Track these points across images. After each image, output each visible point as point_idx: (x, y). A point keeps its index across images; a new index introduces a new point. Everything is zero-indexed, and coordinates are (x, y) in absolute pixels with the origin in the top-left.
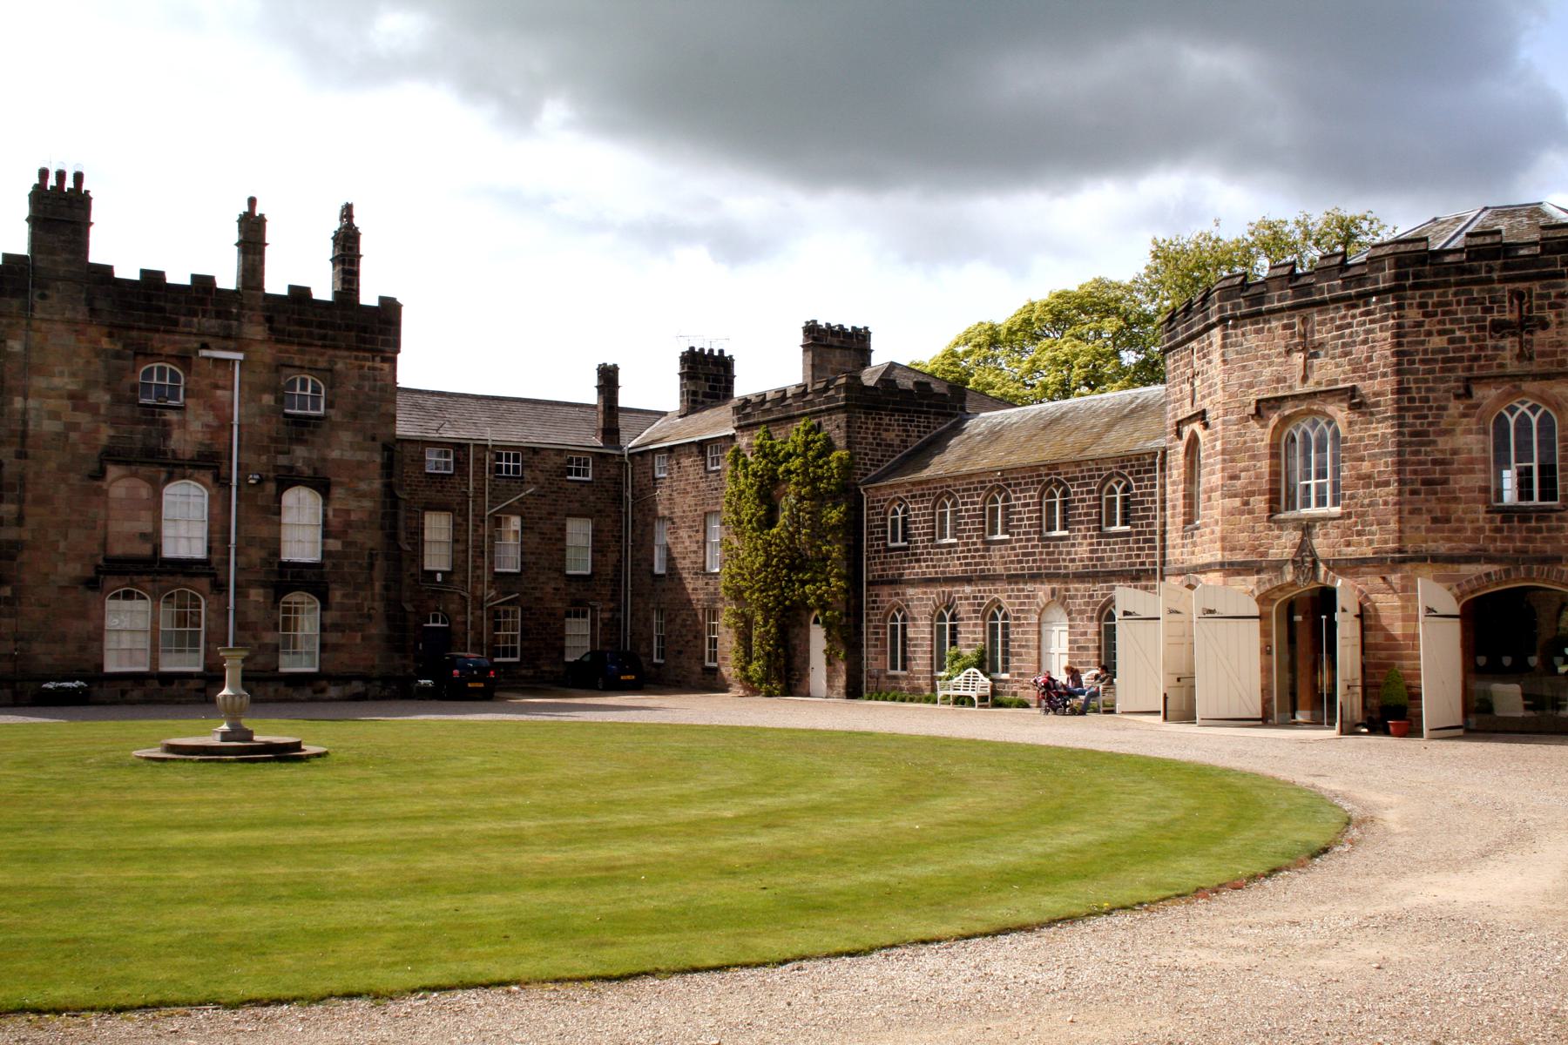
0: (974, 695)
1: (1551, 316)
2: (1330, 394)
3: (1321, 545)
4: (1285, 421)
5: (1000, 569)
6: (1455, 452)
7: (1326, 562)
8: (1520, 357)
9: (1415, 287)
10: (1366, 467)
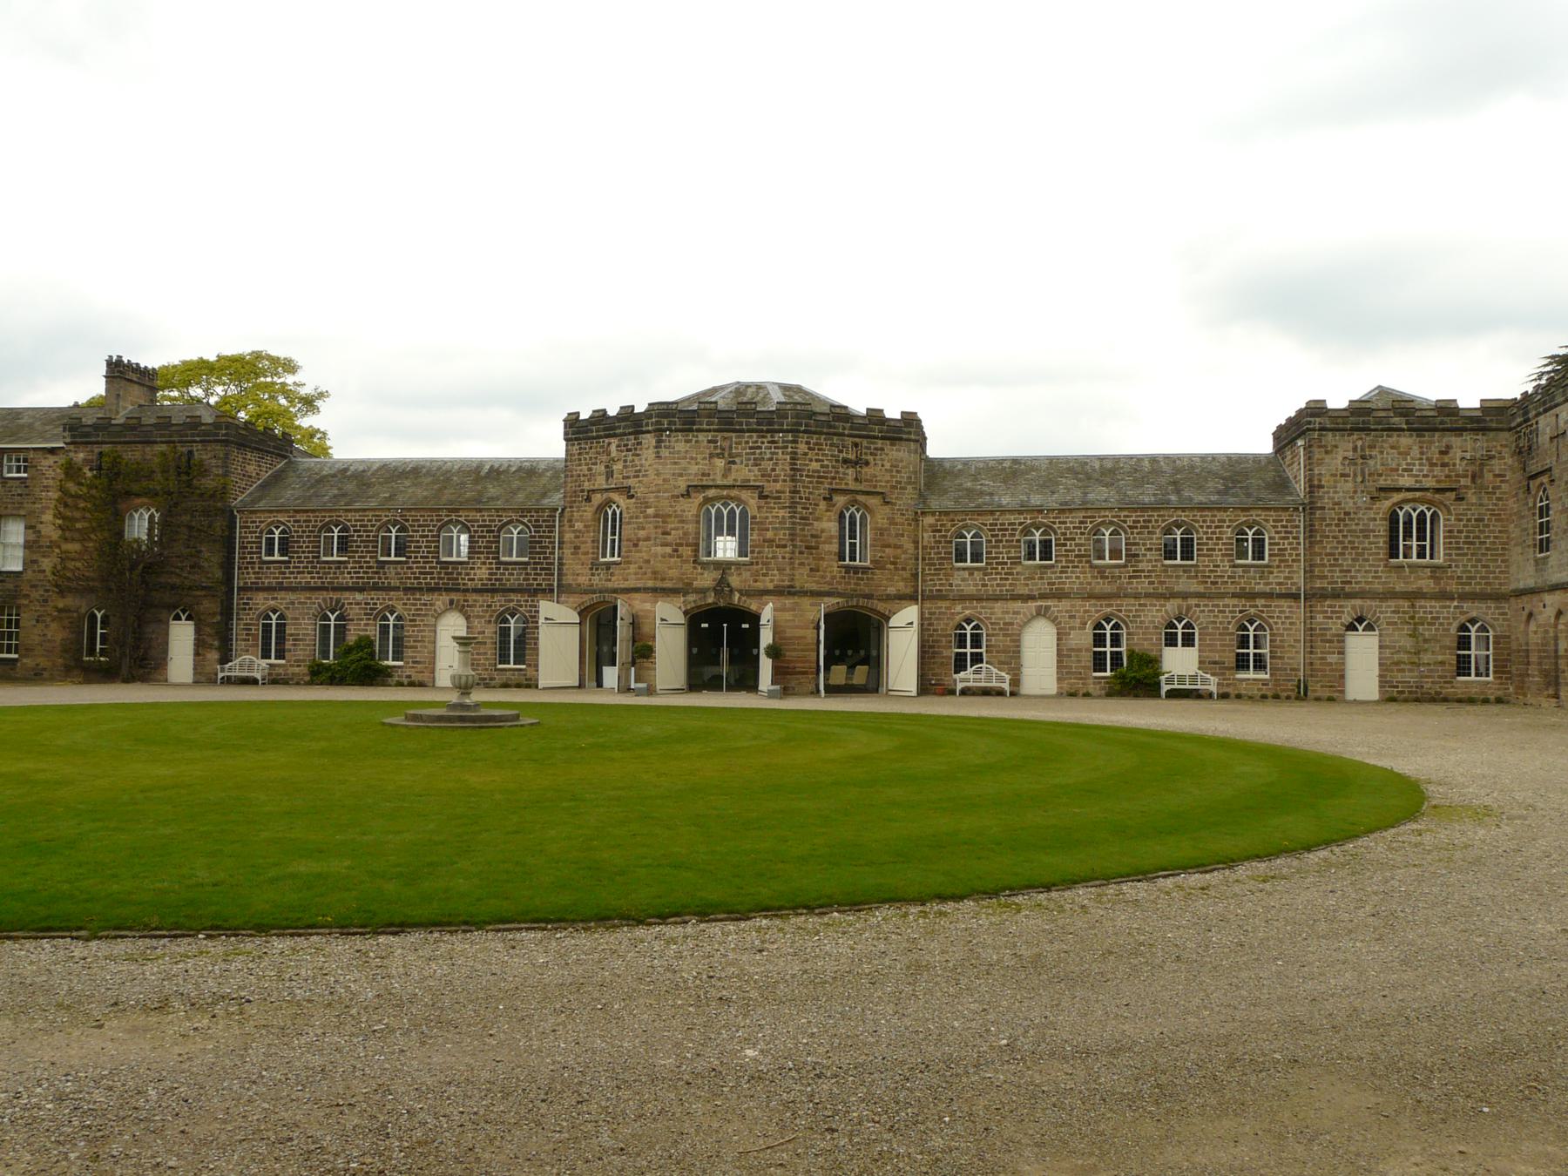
0: (258, 676)
1: (870, 458)
2: (745, 486)
3: (734, 581)
4: (707, 500)
5: (395, 583)
6: (823, 531)
7: (740, 591)
8: (856, 480)
9: (805, 432)
10: (769, 535)
